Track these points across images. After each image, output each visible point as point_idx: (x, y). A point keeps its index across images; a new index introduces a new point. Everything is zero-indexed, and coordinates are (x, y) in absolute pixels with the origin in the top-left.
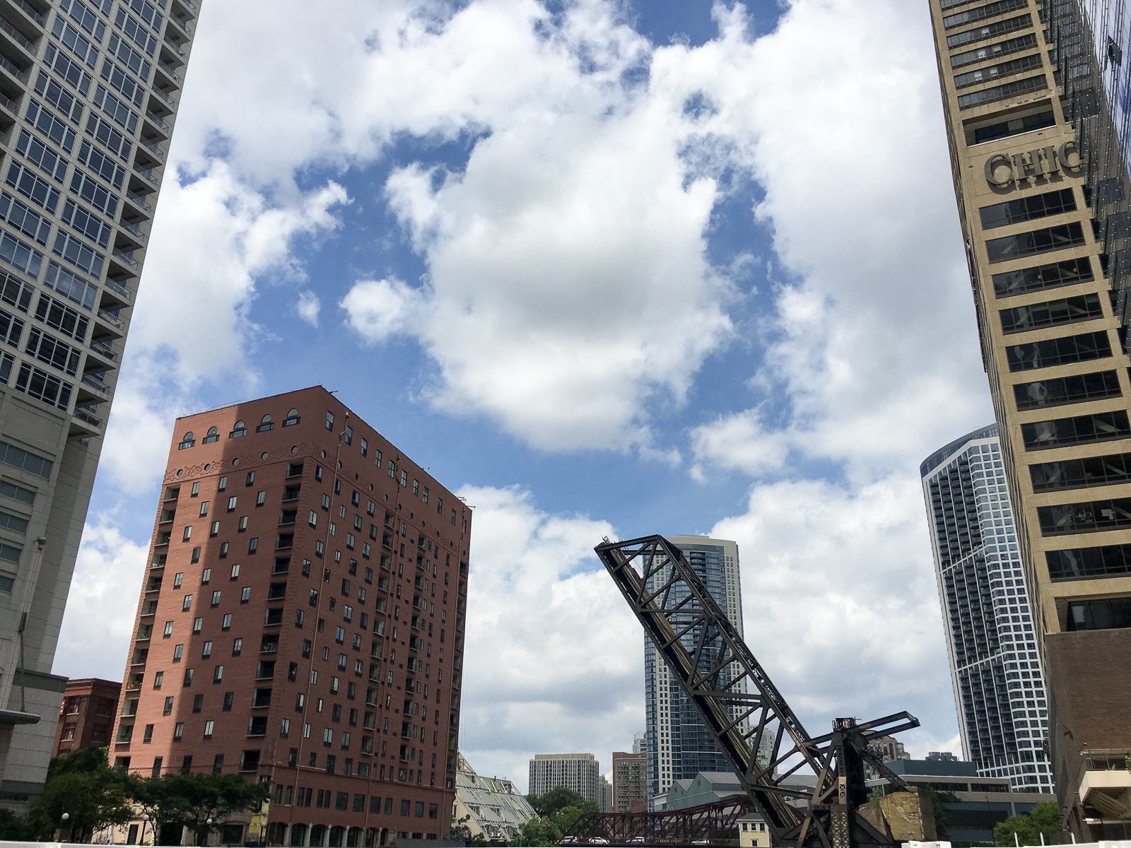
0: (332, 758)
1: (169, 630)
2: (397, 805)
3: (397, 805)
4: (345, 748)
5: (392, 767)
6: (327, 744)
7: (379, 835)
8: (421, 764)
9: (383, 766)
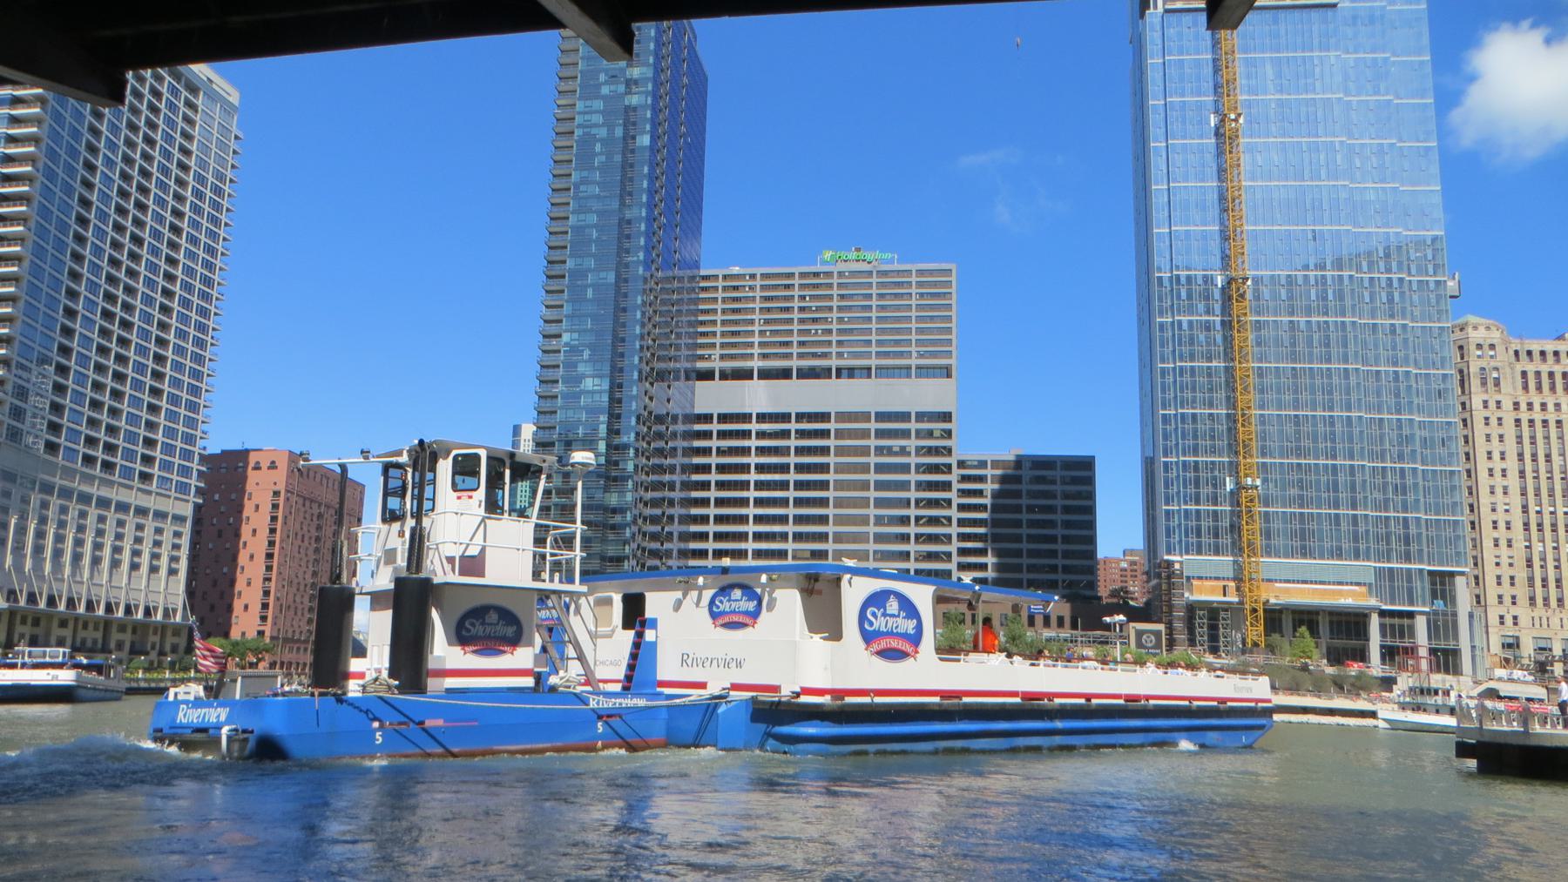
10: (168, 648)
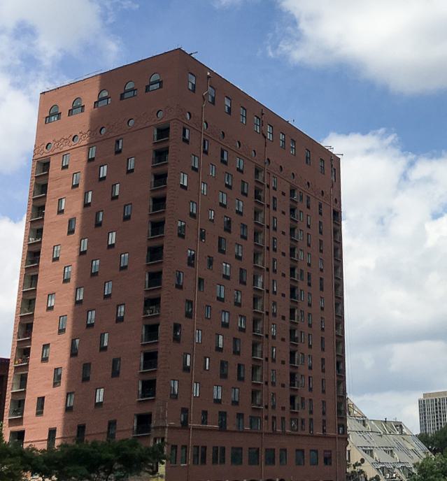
0: (223, 415)
1: (52, 303)
2: (291, 455)
3: (291, 455)
4: (235, 403)
5: (283, 419)
6: (218, 401)
8: (311, 412)
9: (274, 418)
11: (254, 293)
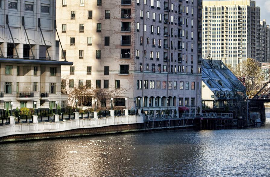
4: (158, 59)
6: (152, 59)
7: (172, 99)
8: (187, 62)
10: (47, 89)
11: (161, 97)
